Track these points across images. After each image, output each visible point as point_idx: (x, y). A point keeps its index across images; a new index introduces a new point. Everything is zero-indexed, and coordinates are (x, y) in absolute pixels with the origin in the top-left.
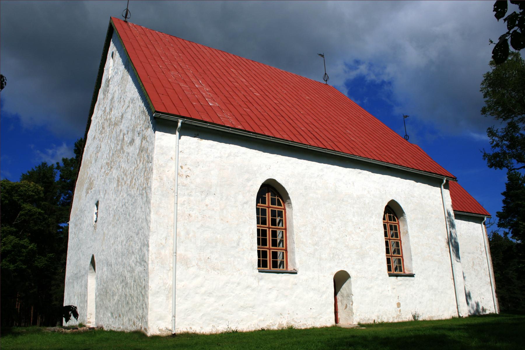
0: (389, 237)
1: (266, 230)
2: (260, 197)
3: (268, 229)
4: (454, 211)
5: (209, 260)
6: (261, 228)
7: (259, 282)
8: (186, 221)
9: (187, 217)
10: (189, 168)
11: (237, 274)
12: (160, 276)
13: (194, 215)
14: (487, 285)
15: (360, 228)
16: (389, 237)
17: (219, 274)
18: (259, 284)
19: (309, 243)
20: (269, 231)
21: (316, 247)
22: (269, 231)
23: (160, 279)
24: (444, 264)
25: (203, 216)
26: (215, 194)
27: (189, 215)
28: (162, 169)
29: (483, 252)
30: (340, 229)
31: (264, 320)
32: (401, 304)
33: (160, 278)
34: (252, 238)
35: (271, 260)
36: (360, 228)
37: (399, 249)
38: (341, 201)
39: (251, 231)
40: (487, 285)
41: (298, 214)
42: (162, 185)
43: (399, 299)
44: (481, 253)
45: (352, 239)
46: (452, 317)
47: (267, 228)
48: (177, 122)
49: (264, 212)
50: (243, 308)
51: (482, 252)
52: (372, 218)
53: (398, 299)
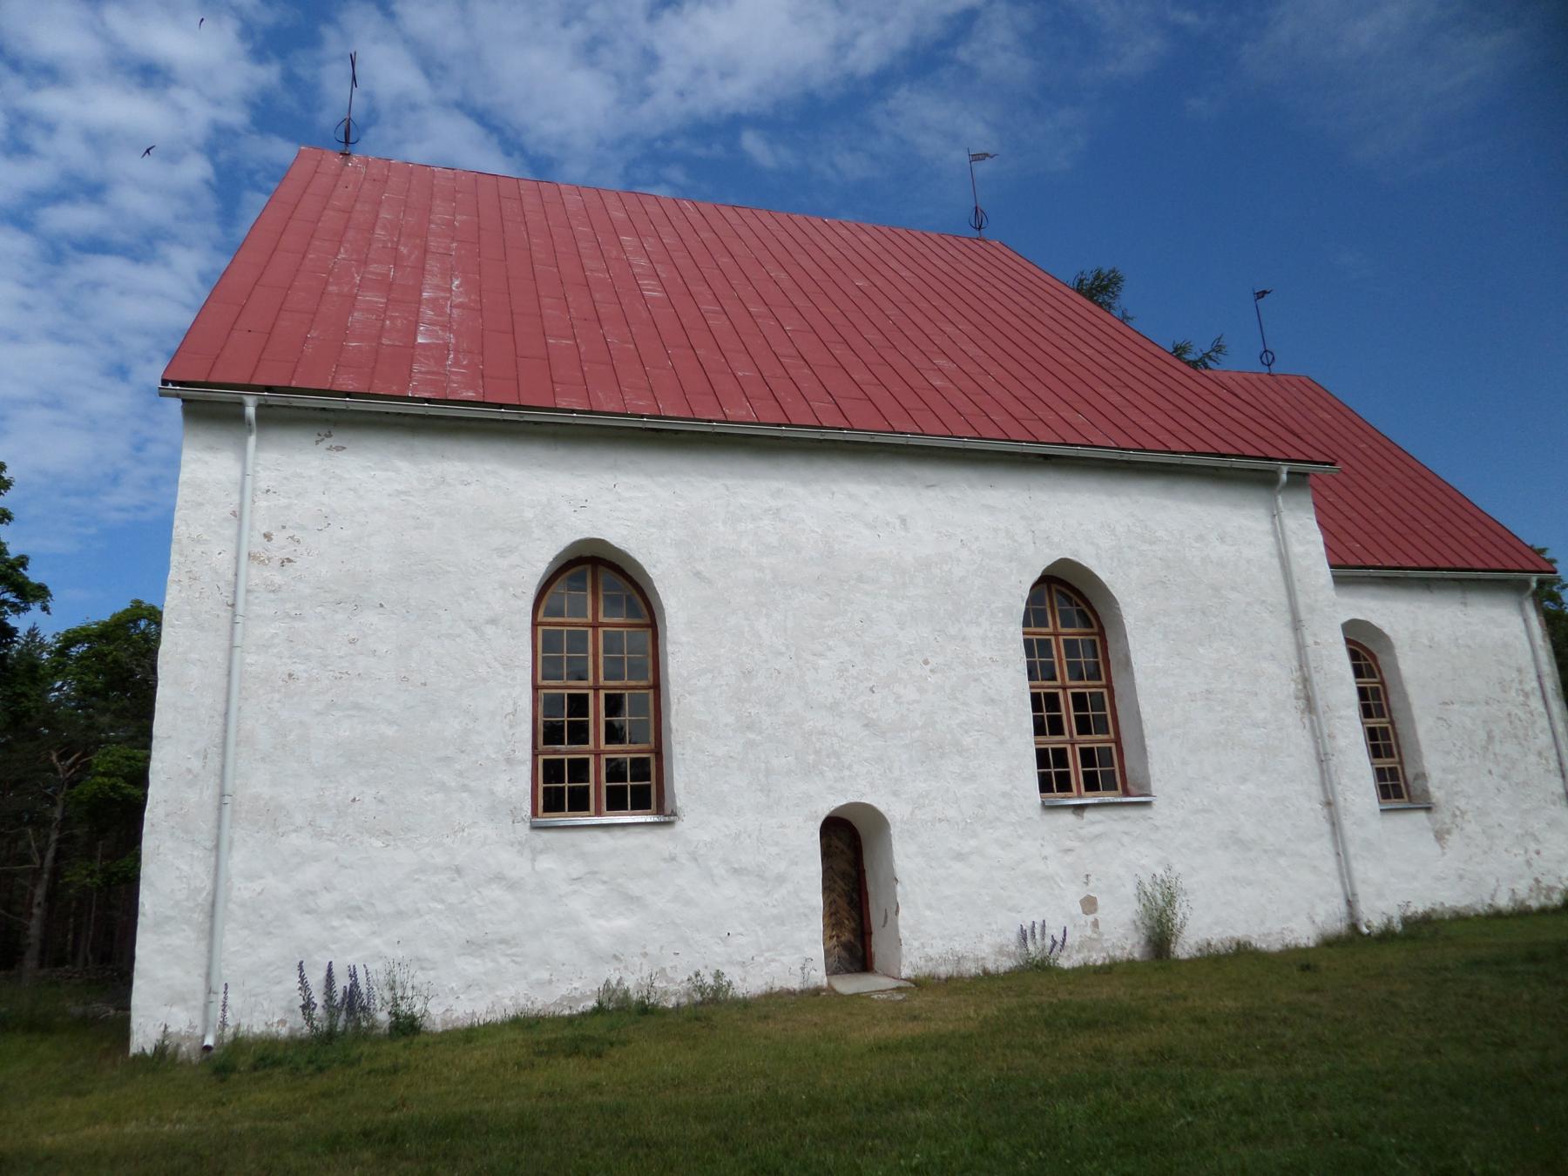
0: (1063, 679)
1: (1057, 694)
2: (1034, 616)
3: (1061, 692)
4: (1332, 567)
5: (357, 804)
6: (1042, 691)
7: (533, 860)
8: (277, 696)
9: (281, 683)
10: (292, 538)
11: (453, 842)
12: (177, 868)
13: (305, 675)
14: (1553, 807)
15: (926, 662)
16: (1063, 679)
17: (387, 846)
18: (533, 869)
19: (726, 725)
20: (596, 697)
21: (751, 736)
22: (596, 697)
23: (177, 878)
24: (1290, 756)
25: (339, 675)
26: (381, 605)
27: (290, 675)
28: (199, 549)
29: (1531, 697)
30: (847, 670)
31: (550, 982)
32: (1100, 902)
33: (178, 873)
34: (511, 727)
35: (604, 784)
36: (926, 662)
37: (1060, 718)
38: (852, 582)
39: (511, 702)
40: (1554, 804)
41: (684, 639)
42: (197, 595)
43: (1091, 884)
44: (1521, 698)
45: (895, 701)
46: (1238, 944)
47: (589, 688)
48: (242, 405)
49: (1045, 646)
50: (473, 947)
51: (1526, 695)
52: (978, 624)
53: (1087, 884)
